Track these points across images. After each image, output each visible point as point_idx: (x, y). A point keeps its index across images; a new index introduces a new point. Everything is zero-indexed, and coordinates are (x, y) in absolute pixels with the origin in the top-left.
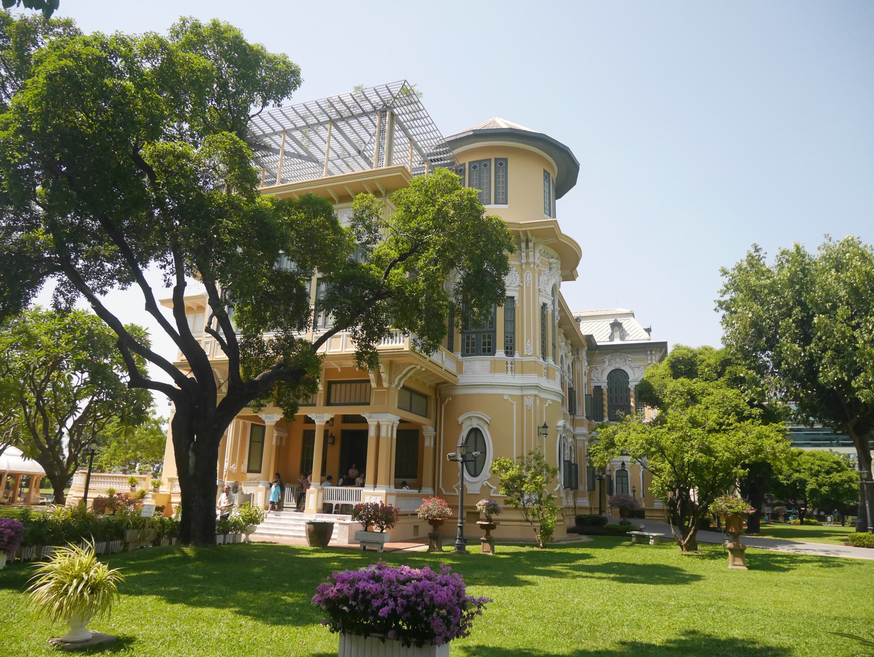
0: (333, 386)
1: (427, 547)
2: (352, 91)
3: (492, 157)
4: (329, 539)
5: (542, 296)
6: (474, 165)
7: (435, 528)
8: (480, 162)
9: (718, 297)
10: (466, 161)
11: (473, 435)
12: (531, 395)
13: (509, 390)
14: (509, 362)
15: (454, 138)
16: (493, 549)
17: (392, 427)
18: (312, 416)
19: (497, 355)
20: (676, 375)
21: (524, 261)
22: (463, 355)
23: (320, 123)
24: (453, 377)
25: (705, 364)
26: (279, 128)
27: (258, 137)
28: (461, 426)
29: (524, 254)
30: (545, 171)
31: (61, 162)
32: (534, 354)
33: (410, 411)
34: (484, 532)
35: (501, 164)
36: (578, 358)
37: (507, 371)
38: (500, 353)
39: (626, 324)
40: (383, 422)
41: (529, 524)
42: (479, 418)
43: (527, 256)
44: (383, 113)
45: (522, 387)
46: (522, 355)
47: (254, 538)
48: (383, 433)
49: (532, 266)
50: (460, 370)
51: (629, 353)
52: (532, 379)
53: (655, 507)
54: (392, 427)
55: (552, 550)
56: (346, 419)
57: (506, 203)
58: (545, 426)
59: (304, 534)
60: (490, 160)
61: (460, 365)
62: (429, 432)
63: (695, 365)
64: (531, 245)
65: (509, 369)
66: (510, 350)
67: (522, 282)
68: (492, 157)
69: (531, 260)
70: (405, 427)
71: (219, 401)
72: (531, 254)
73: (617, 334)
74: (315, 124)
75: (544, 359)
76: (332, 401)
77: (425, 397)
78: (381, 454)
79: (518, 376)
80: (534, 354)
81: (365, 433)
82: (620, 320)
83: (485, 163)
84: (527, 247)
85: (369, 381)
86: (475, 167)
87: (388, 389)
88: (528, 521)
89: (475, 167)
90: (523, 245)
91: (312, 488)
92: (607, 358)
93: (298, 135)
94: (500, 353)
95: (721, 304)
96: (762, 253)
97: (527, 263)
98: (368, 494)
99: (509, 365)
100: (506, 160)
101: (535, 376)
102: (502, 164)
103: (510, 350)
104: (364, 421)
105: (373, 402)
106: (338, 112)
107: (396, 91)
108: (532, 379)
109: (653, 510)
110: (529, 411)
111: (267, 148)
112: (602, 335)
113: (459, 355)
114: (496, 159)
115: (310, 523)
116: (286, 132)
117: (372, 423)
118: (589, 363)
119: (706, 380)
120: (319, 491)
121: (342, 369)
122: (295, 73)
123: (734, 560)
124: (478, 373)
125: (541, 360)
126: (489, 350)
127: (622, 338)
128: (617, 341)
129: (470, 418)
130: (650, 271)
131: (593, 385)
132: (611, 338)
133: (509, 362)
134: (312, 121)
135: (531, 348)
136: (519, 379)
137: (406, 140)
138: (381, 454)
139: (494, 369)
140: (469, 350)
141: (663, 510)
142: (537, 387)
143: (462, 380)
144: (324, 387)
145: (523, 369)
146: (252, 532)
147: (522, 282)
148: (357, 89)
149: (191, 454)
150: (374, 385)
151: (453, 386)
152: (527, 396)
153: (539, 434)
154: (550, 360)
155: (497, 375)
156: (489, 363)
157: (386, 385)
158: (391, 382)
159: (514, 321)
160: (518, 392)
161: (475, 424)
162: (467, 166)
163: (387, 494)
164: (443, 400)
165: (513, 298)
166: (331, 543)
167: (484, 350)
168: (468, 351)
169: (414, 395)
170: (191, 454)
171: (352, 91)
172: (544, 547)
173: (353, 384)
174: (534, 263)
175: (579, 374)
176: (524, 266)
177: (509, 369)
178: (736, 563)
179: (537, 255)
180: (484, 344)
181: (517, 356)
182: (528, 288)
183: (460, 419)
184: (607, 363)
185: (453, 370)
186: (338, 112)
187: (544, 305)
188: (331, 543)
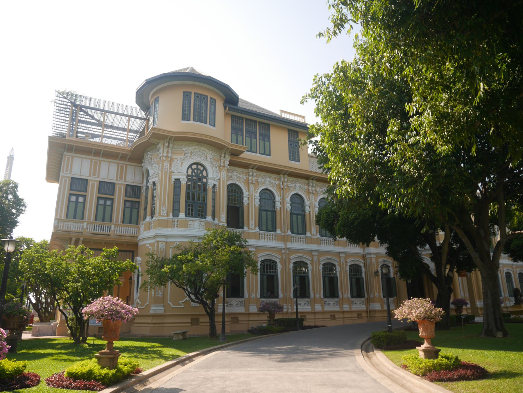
8: (201, 95)
12: (163, 242)
14: (176, 221)
19: (207, 219)
30: (184, 92)
31: (516, 70)
32: (160, 215)
35: (187, 95)
37: (174, 226)
38: (209, 218)
46: (219, 221)
60: (191, 93)
65: (176, 225)
71: (494, 246)
79: (309, 245)
94: (209, 218)
114: (195, 93)
133: (176, 221)
142: (157, 236)
152: (161, 241)
159: (174, 194)
176: (221, 167)
177: (176, 225)
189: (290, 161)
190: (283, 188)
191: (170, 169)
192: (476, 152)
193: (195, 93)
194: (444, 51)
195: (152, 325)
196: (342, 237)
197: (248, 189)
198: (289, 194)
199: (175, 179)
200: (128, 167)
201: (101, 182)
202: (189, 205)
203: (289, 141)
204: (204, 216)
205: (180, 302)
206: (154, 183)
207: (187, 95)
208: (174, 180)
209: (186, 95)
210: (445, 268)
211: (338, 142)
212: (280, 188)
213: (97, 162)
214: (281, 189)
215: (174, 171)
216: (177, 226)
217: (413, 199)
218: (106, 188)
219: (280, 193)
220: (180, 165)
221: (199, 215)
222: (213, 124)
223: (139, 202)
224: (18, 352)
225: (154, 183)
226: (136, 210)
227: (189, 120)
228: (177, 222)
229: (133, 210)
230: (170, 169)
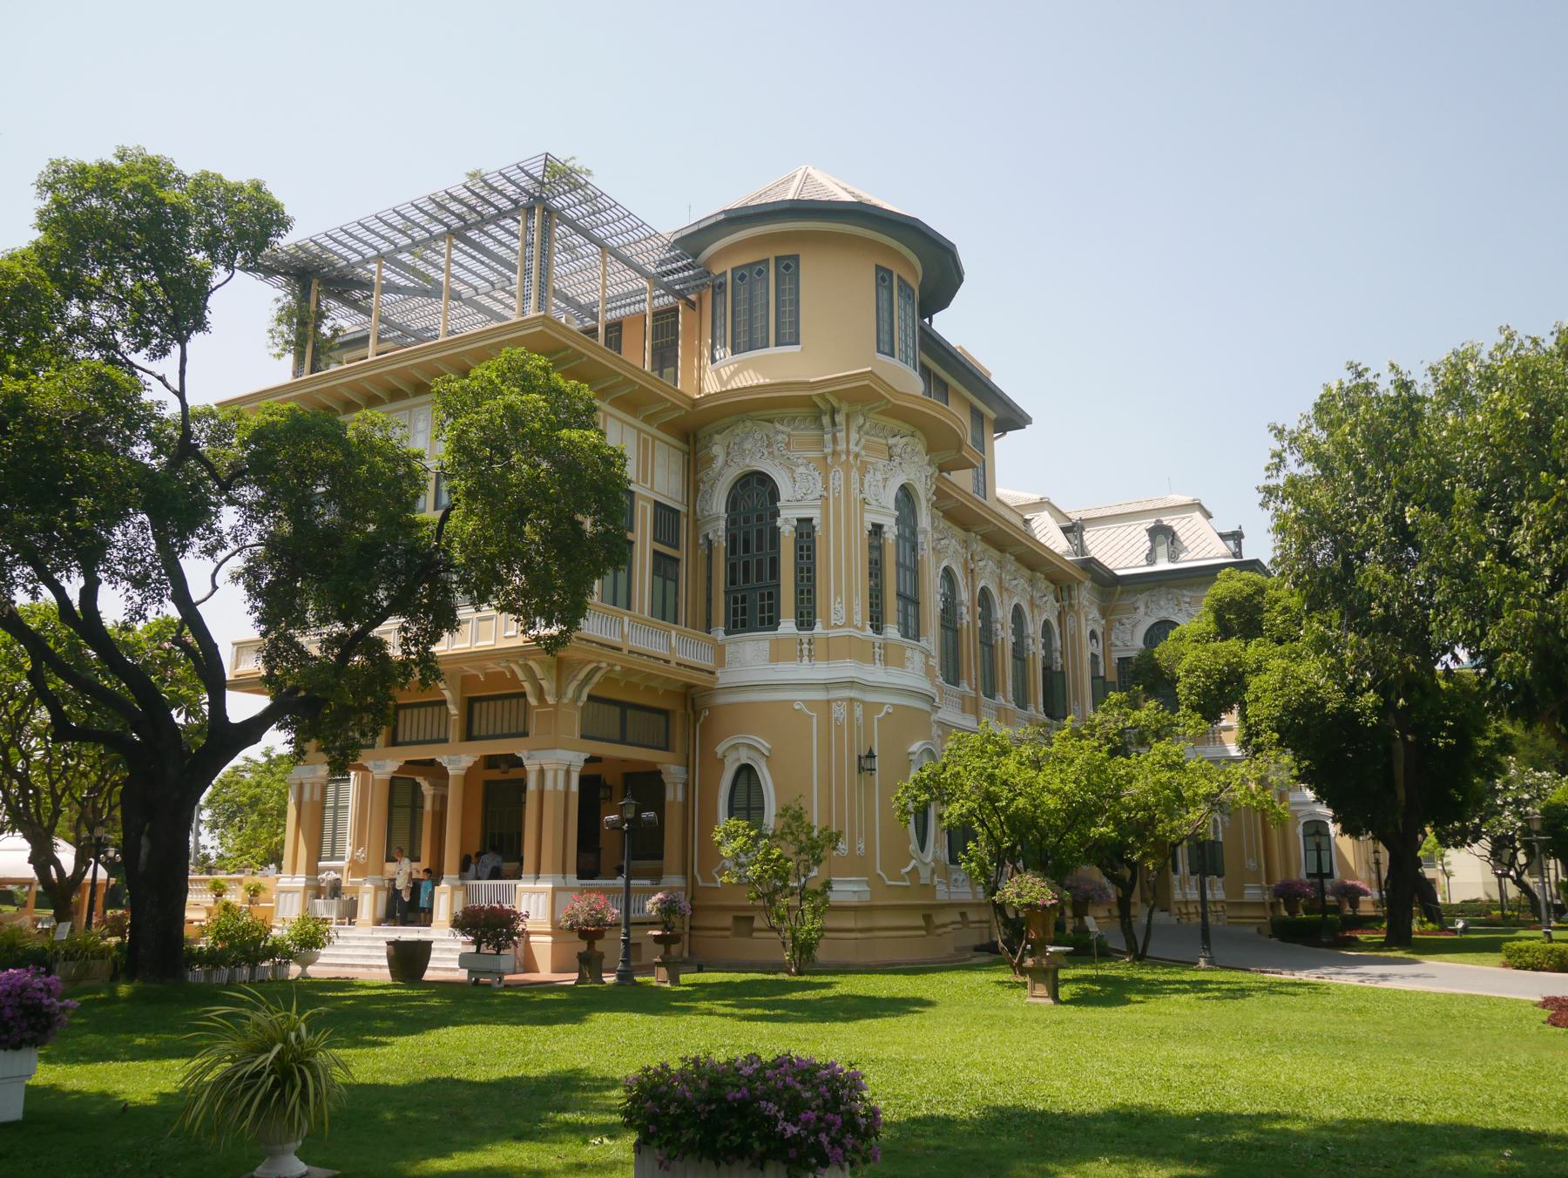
0: (477, 706)
1: (575, 976)
2: (465, 179)
3: (770, 254)
4: (424, 967)
5: (870, 511)
6: (740, 274)
7: (591, 945)
9: (1263, 483)
10: (724, 268)
11: (744, 777)
12: (842, 700)
13: (818, 692)
14: (805, 640)
15: (696, 228)
16: (675, 981)
17: (568, 773)
18: (443, 760)
19: (781, 629)
20: (1225, 632)
21: (828, 450)
22: (727, 633)
23: (434, 238)
24: (705, 676)
25: (1278, 608)
26: (371, 253)
27: (353, 266)
28: (722, 761)
29: (828, 437)
30: (878, 268)
32: (849, 623)
33: (623, 741)
34: (661, 948)
35: (787, 267)
36: (1071, 605)
37: (802, 656)
38: (787, 626)
39: (1188, 528)
40: (553, 766)
41: (775, 935)
42: (750, 747)
43: (835, 440)
44: (529, 210)
45: (827, 686)
46: (827, 626)
47: (314, 971)
48: (549, 785)
49: (844, 457)
50: (720, 660)
51: (1185, 587)
52: (846, 669)
53: (1247, 898)
54: (568, 773)
55: (766, 977)
56: (491, 762)
57: (797, 343)
58: (871, 756)
59: (385, 962)
61: (719, 652)
62: (673, 773)
63: (1260, 610)
64: (839, 418)
65: (806, 652)
66: (805, 620)
67: (826, 489)
68: (770, 254)
69: (842, 447)
70: (594, 770)
72: (841, 435)
73: (1162, 550)
74: (493, 216)
75: (877, 627)
76: (475, 733)
77: (665, 713)
78: (549, 822)
79: (821, 665)
80: (849, 623)
81: (521, 785)
82: (1166, 521)
83: (759, 268)
84: (834, 423)
85: (524, 695)
86: (742, 278)
87: (555, 706)
88: (773, 928)
89: (742, 278)
90: (826, 420)
91: (444, 885)
92: (1141, 601)
93: (405, 257)
95: (1269, 491)
96: (1369, 376)
97: (834, 453)
98: (525, 891)
99: (805, 646)
100: (796, 258)
101: (848, 663)
102: (789, 266)
103: (805, 620)
104: (516, 762)
105: (533, 730)
106: (460, 217)
107: (537, 172)
108: (846, 669)
109: (1242, 904)
110: (840, 728)
111: (366, 285)
112: (1123, 552)
113: (719, 634)
114: (777, 259)
115: (389, 943)
116: (380, 257)
117: (531, 767)
118: (1104, 613)
119: (1280, 642)
120: (454, 888)
121: (486, 675)
122: (275, 208)
123: (1033, 988)
124: (753, 664)
125: (869, 632)
126: (771, 620)
127: (1173, 558)
128: (1163, 565)
129: (735, 747)
130: (1151, 435)
131: (1116, 656)
132: (1151, 558)
133: (805, 640)
134: (419, 234)
135: (843, 613)
136: (822, 671)
137: (593, 248)
138: (549, 822)
139: (775, 657)
140: (739, 623)
141: (1263, 904)
142: (851, 684)
143: (725, 678)
144: (461, 710)
145: (831, 650)
146: (312, 962)
147: (826, 489)
148: (473, 176)
149: (144, 841)
150: (533, 701)
151: (709, 691)
152: (836, 700)
153: (861, 769)
154: (892, 632)
155: (781, 665)
156: (767, 644)
157: (551, 700)
158: (560, 694)
160: (820, 696)
161: (744, 757)
162: (729, 275)
163: (555, 890)
164: (697, 714)
165: (811, 520)
166: (429, 975)
167: (762, 621)
168: (735, 626)
169: (629, 712)
170: (144, 841)
171: (465, 179)
172: (800, 973)
173: (492, 699)
174: (848, 453)
175: (1073, 636)
177: (806, 652)
178: (1037, 993)
179: (854, 436)
180: (762, 611)
181: (819, 628)
182: (837, 500)
183: (720, 749)
184: (1142, 609)
185: (708, 664)
186: (460, 217)
187: (877, 529)
188: (429, 975)
192: (1305, 777)
194: (1469, 546)
195: (859, 935)
196: (464, 960)
199: (874, 525)
204: (772, 623)
205: (904, 871)
207: (787, 267)
215: (870, 499)
216: (810, 656)
221: (762, 623)
222: (887, 349)
224: (638, 979)
228: (810, 643)
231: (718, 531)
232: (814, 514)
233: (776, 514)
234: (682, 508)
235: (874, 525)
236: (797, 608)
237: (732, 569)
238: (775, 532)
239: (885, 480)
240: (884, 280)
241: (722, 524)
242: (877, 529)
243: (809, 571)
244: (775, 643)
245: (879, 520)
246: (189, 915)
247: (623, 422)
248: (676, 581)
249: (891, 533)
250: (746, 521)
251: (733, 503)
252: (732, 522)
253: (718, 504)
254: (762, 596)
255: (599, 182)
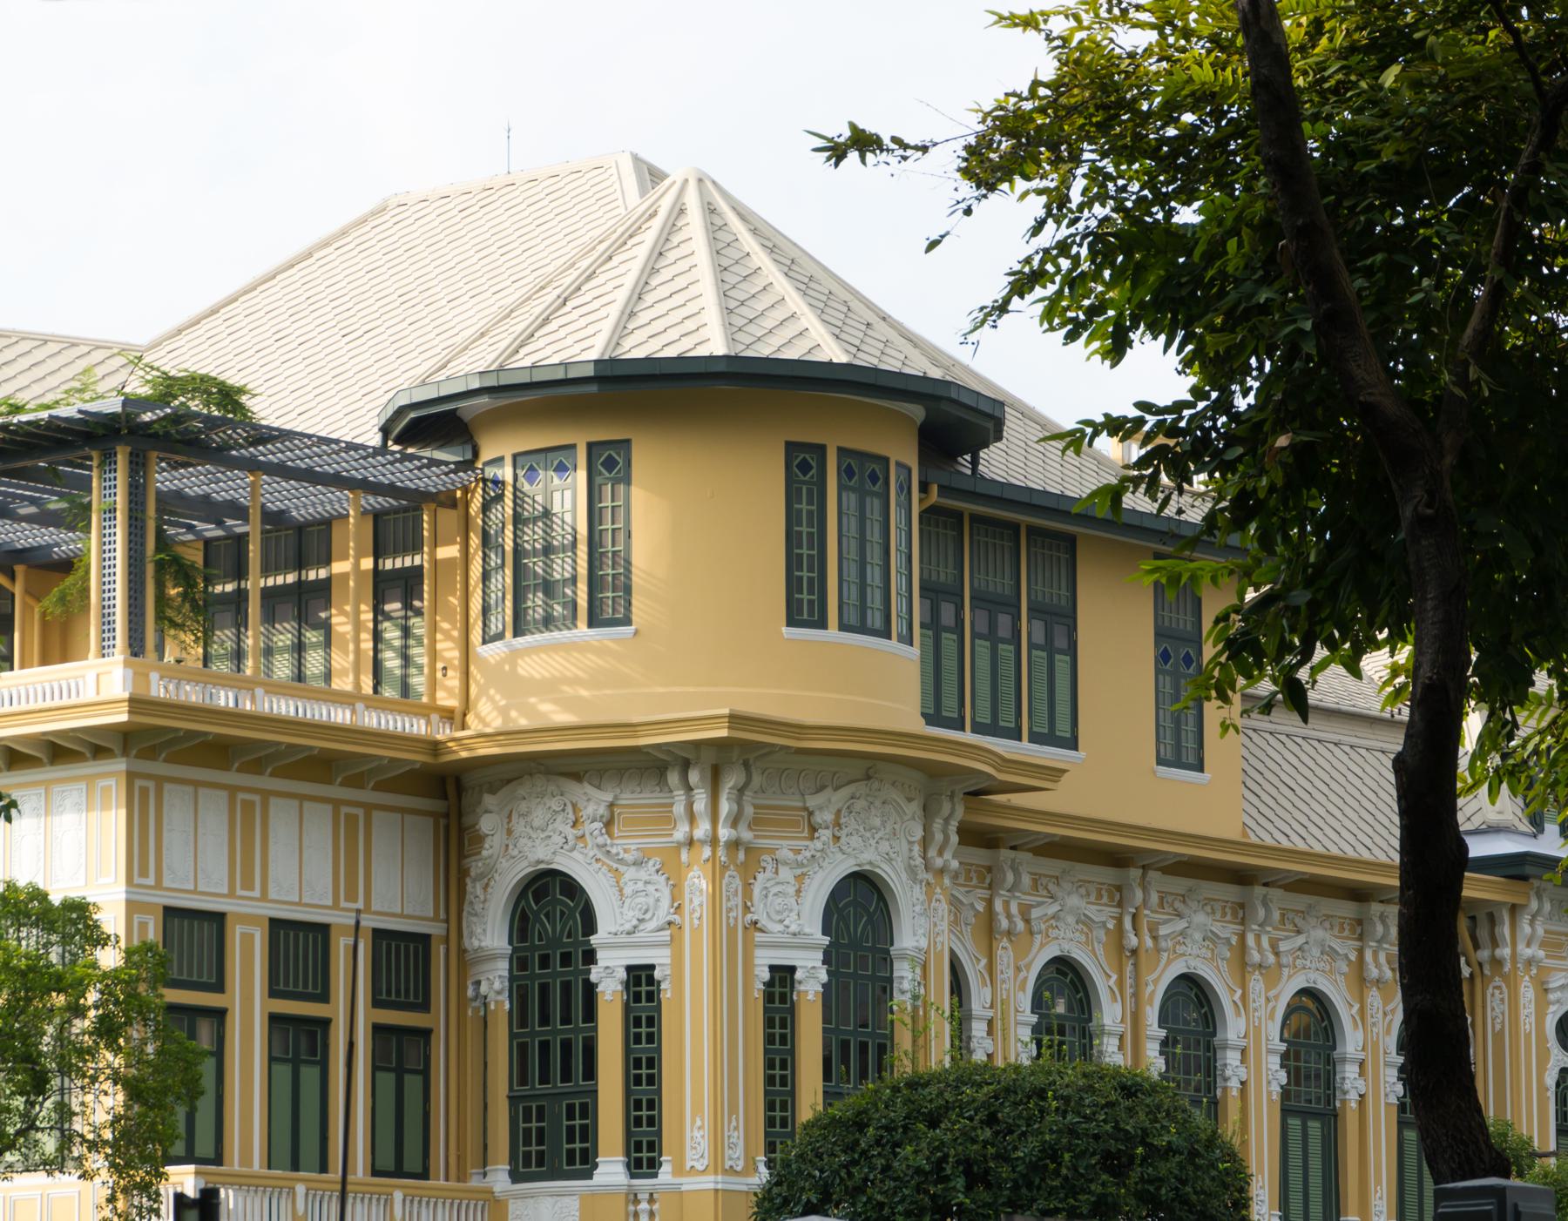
22: (516, 1177)
30: (791, 448)
38: (611, 1170)
46: (679, 1170)
60: (821, 450)
100: (628, 441)
113: (499, 1179)
114: (841, 450)
181: (665, 1174)
187: (783, 976)
189: (1163, 770)
190: (1134, 952)
191: (747, 909)
193: (841, 450)
197: (990, 967)
198: (1156, 982)
199: (773, 969)
200: (377, 816)
201: (276, 924)
202: (783, 1083)
203: (1161, 634)
206: (641, 980)
208: (766, 976)
209: (803, 464)
210: (61, 496)
211: (1104, 127)
212: (1121, 947)
213: (252, 803)
214: (1127, 956)
215: (764, 922)
217: (1472, 103)
218: (298, 949)
219: (1120, 983)
220: (791, 890)
221: (571, 1161)
223: (426, 1034)
225: (641, 980)
226: (419, 1079)
227: (822, 624)
229: (408, 1078)
230: (747, 909)
231: (495, 981)
232: (659, 958)
233: (590, 957)
234: (435, 929)
235: (773, 969)
236: (628, 1134)
237: (520, 1053)
238: (590, 990)
239: (800, 878)
240: (805, 467)
241: (503, 967)
242: (783, 976)
243: (651, 1063)
244: (590, 1203)
245: (783, 958)
246: (1466, 893)
247: (302, 798)
248: (425, 1073)
249: (812, 978)
250: (545, 961)
251: (521, 925)
252: (519, 962)
253: (491, 934)
254: (571, 1108)
255: (40, 1177)
